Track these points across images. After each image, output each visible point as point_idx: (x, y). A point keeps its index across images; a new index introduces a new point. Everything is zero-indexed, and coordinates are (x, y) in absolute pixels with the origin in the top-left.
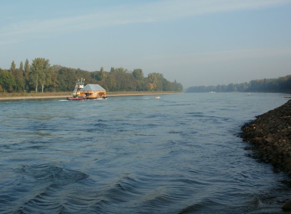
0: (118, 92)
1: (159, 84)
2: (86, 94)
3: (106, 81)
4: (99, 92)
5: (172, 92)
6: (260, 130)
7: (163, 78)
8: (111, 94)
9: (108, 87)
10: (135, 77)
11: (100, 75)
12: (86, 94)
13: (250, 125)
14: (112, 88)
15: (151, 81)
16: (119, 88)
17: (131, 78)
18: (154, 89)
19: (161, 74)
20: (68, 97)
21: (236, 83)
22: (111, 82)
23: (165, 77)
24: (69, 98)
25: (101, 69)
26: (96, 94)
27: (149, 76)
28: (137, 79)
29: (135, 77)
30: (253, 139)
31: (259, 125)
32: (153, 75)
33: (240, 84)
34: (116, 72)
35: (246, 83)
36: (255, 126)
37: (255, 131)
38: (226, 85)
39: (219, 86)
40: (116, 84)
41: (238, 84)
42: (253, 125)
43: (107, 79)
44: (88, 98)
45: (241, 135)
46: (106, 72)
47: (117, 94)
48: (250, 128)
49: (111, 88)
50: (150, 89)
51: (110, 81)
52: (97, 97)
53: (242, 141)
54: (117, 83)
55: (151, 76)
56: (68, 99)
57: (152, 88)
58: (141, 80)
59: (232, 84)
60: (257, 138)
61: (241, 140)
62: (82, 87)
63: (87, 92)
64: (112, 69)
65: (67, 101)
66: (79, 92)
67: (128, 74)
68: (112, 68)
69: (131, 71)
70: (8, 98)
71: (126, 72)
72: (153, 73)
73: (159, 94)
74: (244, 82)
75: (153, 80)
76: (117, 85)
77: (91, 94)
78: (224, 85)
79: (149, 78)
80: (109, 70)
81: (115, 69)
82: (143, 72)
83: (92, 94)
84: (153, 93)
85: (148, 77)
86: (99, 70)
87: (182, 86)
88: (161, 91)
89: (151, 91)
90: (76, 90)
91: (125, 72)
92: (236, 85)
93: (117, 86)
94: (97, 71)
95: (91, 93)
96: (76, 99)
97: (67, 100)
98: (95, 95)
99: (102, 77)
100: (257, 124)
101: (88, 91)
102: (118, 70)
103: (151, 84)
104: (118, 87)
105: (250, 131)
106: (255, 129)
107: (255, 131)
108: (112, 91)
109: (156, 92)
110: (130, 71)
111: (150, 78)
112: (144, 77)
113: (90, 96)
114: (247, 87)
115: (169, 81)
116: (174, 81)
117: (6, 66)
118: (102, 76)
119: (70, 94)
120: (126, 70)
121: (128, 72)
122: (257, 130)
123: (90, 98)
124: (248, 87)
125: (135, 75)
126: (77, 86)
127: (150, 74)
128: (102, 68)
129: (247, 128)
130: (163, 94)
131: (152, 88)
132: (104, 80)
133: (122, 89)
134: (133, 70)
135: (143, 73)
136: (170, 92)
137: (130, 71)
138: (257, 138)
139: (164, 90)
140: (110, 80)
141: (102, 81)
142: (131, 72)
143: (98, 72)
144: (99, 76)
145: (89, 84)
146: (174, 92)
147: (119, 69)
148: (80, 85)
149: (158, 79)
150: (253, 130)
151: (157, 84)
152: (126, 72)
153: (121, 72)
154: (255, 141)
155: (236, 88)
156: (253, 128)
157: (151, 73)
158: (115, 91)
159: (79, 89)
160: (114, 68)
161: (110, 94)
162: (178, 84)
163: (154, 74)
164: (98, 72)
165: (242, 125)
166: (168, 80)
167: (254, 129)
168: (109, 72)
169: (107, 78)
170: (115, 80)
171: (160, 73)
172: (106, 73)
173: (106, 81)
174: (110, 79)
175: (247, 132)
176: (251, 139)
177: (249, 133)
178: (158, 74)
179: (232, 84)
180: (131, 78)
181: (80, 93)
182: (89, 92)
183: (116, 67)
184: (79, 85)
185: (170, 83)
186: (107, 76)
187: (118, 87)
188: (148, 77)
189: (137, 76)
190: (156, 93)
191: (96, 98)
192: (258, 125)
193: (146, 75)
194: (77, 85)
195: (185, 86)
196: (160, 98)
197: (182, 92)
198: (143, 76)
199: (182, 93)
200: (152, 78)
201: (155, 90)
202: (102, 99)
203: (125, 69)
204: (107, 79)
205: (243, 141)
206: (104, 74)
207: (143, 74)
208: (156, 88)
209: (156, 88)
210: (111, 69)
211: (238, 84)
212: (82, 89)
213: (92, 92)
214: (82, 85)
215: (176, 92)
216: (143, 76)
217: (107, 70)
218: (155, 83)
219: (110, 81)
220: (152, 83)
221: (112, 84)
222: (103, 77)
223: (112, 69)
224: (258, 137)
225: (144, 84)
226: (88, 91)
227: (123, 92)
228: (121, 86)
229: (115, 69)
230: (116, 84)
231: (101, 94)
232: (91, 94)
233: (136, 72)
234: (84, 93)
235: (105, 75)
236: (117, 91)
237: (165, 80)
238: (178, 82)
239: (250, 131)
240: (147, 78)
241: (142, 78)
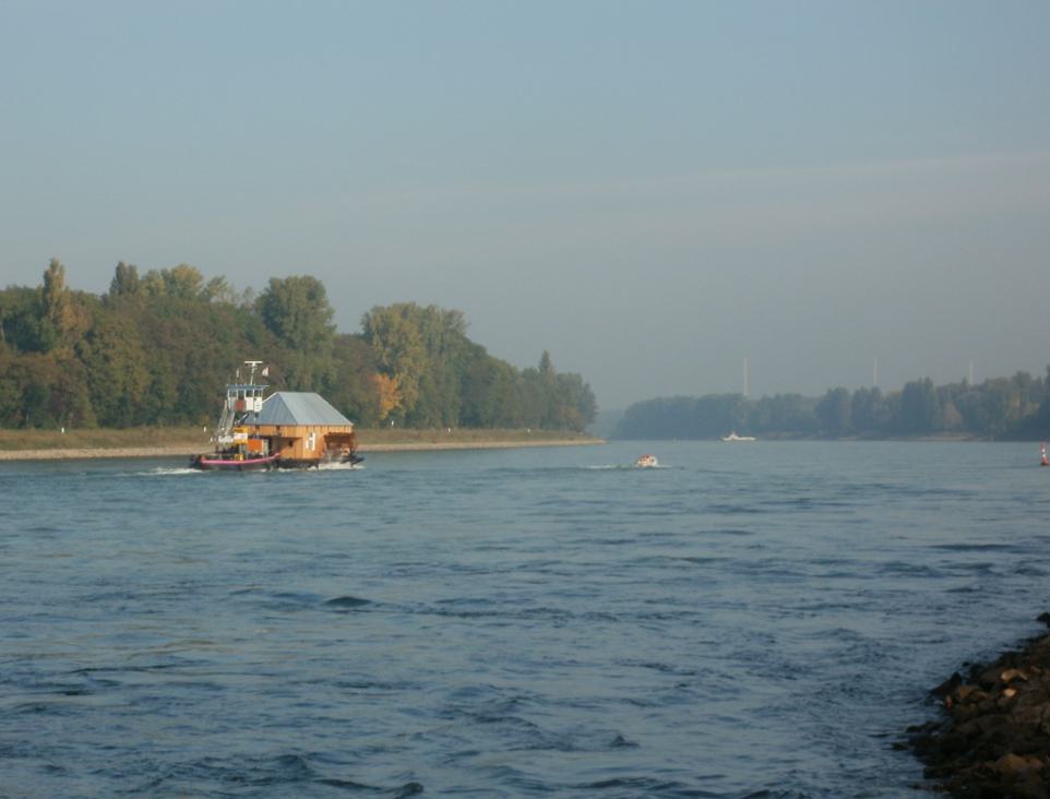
0: (161, 432)
1: (438, 383)
2: (270, 439)
3: (79, 353)
4: (326, 432)
5: (526, 437)
6: (1038, 708)
7: (467, 341)
8: (115, 446)
9: (96, 397)
10: (275, 328)
11: (39, 317)
12: (270, 439)
13: (988, 677)
14: (122, 401)
15: (386, 361)
16: (169, 405)
17: (251, 339)
18: (403, 413)
19: (451, 315)
20: (200, 457)
21: (958, 380)
22: (117, 364)
23: (474, 335)
24: (204, 461)
25: (48, 278)
26: (313, 439)
27: (368, 326)
28: (291, 343)
29: (275, 328)
30: (989, 764)
31: (1041, 675)
32: (397, 319)
33: (980, 381)
34: (146, 293)
35: (1021, 379)
36: (1014, 682)
37: (1008, 718)
38: (885, 392)
39: (836, 397)
40: (146, 375)
41: (964, 381)
42: (1005, 676)
43: (85, 345)
44: (279, 463)
45: (918, 743)
46: (81, 293)
47: (153, 443)
48: (984, 694)
49: (116, 403)
50: (378, 412)
51: (107, 359)
52: (317, 456)
53: (919, 779)
54: (153, 372)
55: (385, 330)
56: (196, 462)
57: (388, 405)
58: (316, 350)
59: (928, 383)
60: (1014, 762)
61: (913, 764)
62: (254, 404)
63: (271, 431)
64: (124, 279)
65: (194, 475)
66: (245, 429)
67: (227, 307)
68: (120, 268)
69: (248, 291)
70: (101, 450)
71: (214, 300)
72: (396, 306)
73: (434, 446)
74: (1009, 373)
75: (392, 356)
76: (154, 383)
77: (291, 442)
78: (875, 390)
79: (367, 337)
80: (99, 284)
81: (141, 273)
82: (332, 297)
83: (297, 444)
84: (392, 439)
85: (361, 331)
86: (35, 282)
87: (592, 397)
88: (445, 426)
89: (384, 424)
90: (228, 423)
91: (209, 294)
92: (957, 393)
93: (155, 388)
94: (17, 290)
95: (291, 435)
96: (231, 462)
97: (191, 466)
98: (309, 445)
99: (51, 326)
100: (1028, 671)
101: (278, 427)
102: (161, 281)
103: (379, 378)
104: (161, 397)
105: (981, 713)
106: (1013, 700)
107: (1008, 717)
108: (121, 428)
109: (413, 431)
110: (240, 289)
111: (376, 339)
112: (339, 331)
113: (287, 453)
114: (1032, 408)
115: (503, 363)
116: (540, 358)
117: (4, 288)
118: (55, 321)
119: (203, 440)
120: (217, 282)
121: (227, 297)
122: (1018, 709)
123: (290, 463)
124: (1037, 406)
125: (278, 319)
126: (231, 402)
127: (377, 309)
128: (54, 266)
129: (964, 691)
130: (462, 445)
131: (388, 405)
132: (66, 352)
133: (190, 413)
134: (260, 287)
135: (332, 304)
136: (512, 432)
137: (240, 289)
138: (1014, 762)
139: (472, 419)
140: (109, 352)
141: (50, 355)
142: (252, 300)
143: (26, 292)
144: (30, 319)
145: (281, 390)
146: (536, 437)
147: (170, 279)
148: (249, 395)
149: (429, 346)
150: (999, 709)
151: (421, 379)
152: (214, 300)
153: (181, 295)
154: (998, 776)
155: (952, 414)
156: (1002, 695)
157: (386, 302)
158: (135, 424)
159: (241, 416)
160: (132, 269)
161: (105, 444)
162: (560, 377)
163: (405, 311)
164: (26, 293)
165: (944, 674)
166: (496, 350)
167: (1001, 702)
168: (104, 297)
169: (89, 336)
170: (143, 348)
171: (445, 304)
172: (80, 299)
173: (79, 353)
174: (107, 346)
175: (957, 722)
176: (977, 765)
177: (967, 728)
178: (428, 314)
179: (928, 383)
180: (251, 339)
181: (250, 437)
182: (286, 433)
183: (149, 262)
184: (241, 398)
185: (512, 371)
186: (84, 324)
187: (161, 397)
188: (361, 331)
189: (288, 323)
190: (418, 438)
191: (314, 462)
192: (1033, 673)
193: (346, 319)
194: (233, 395)
195: (612, 397)
196: (659, 463)
197: (589, 436)
198: (332, 329)
199: (586, 442)
200: (392, 339)
201: (411, 419)
202: (347, 466)
203: (205, 283)
204: (85, 345)
205: (928, 775)
206: (67, 310)
207: (330, 314)
208: (412, 408)
209: (418, 404)
210: (113, 274)
211: (964, 381)
212: (257, 415)
213: (299, 432)
214: (256, 394)
215: (549, 437)
216: (332, 329)
217: (90, 278)
218: (411, 371)
219: (107, 359)
220: (388, 371)
221: (119, 376)
222: (59, 332)
223: (124, 279)
224: (1018, 753)
225: (334, 377)
226: (278, 427)
227: (194, 431)
228: (180, 389)
229: (141, 273)
230: (144, 378)
231: (334, 441)
232: (291, 442)
233: (284, 296)
234: (262, 437)
235: (76, 314)
236: (152, 421)
237: (478, 352)
238: (560, 367)
239: (981, 713)
240: (358, 337)
241: (320, 337)
